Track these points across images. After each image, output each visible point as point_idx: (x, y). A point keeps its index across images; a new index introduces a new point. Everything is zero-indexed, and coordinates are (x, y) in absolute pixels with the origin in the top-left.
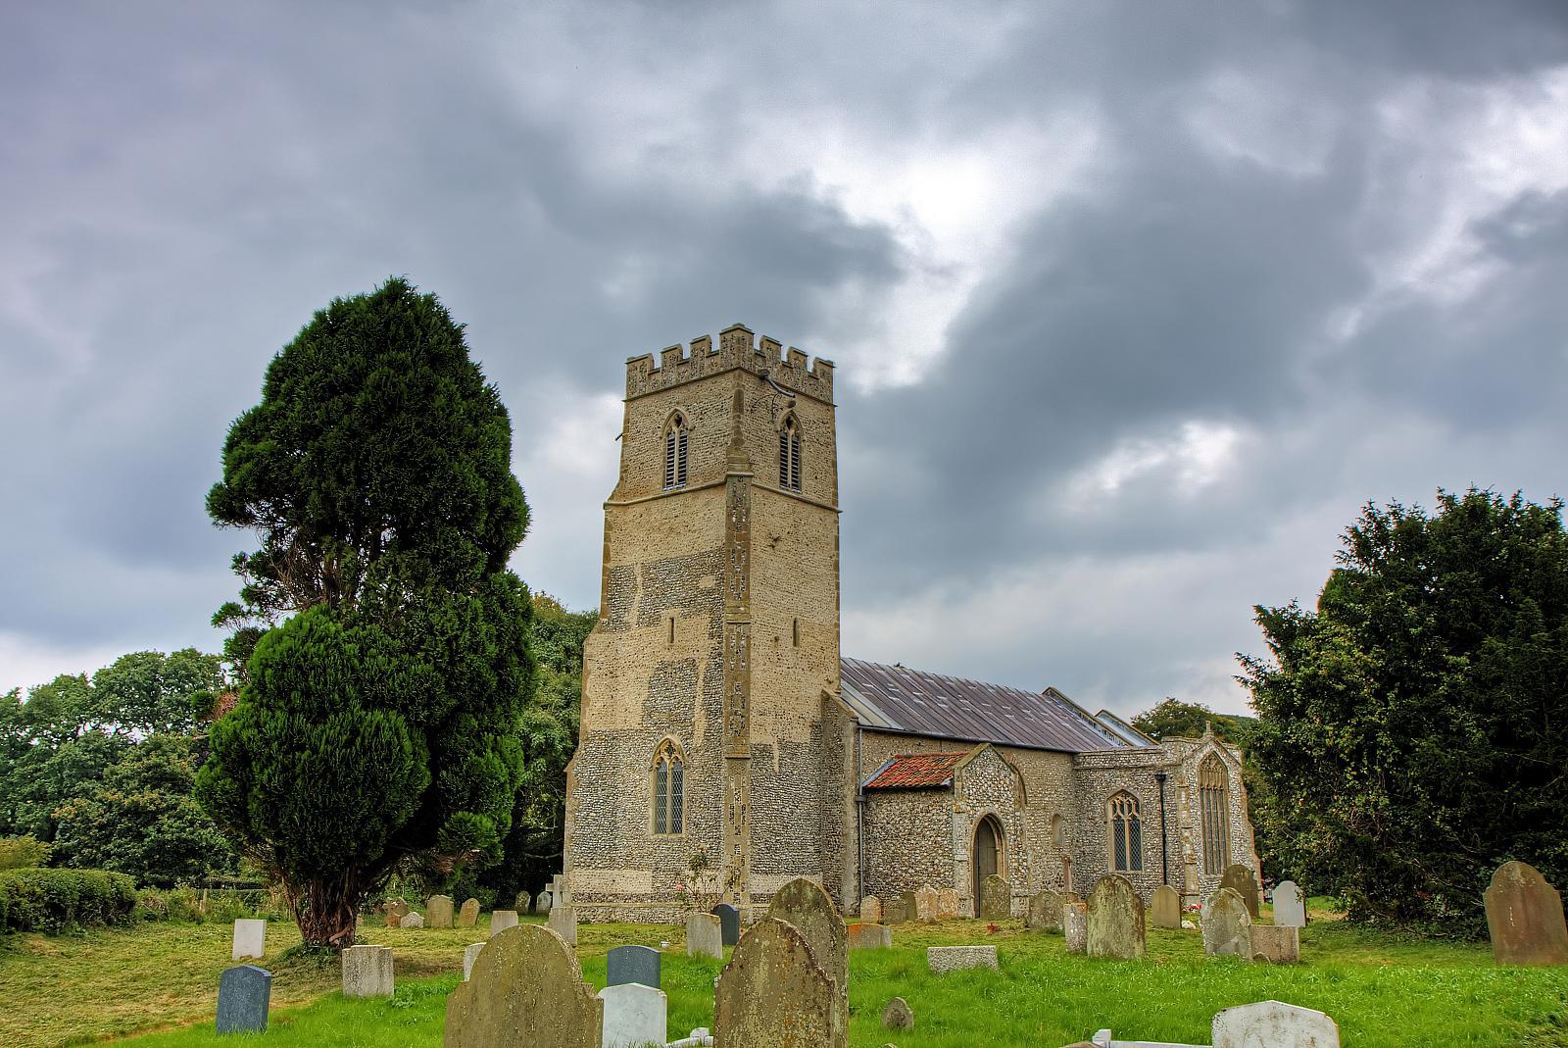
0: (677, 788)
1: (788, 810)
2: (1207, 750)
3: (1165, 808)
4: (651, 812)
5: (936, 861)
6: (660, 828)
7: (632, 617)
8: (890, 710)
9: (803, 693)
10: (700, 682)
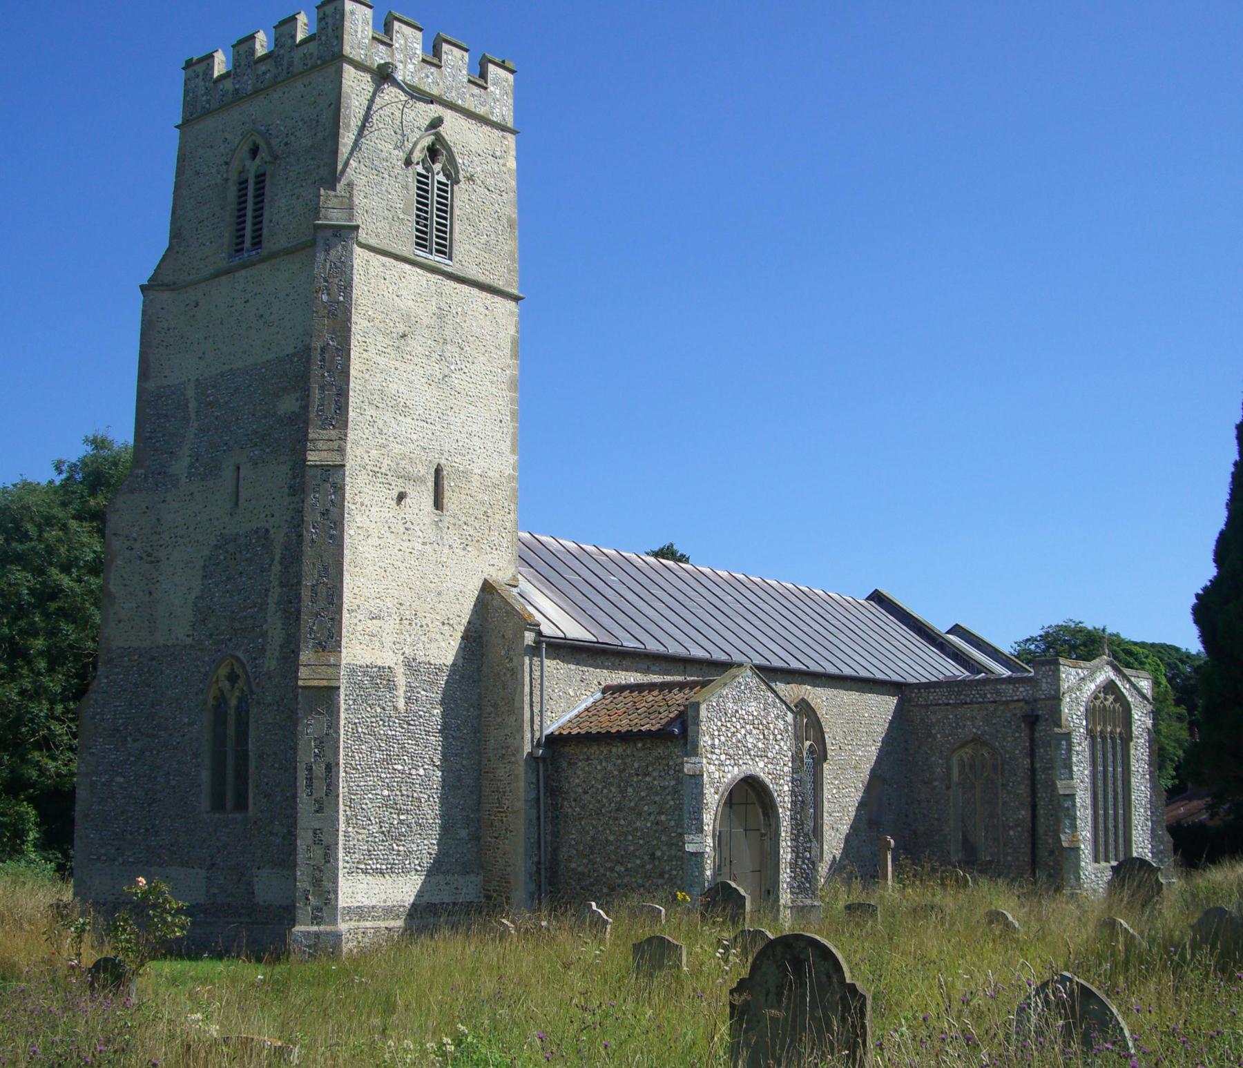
0: (242, 736)
1: (421, 772)
2: (1101, 678)
3: (1038, 765)
4: (205, 776)
5: (658, 853)
6: (218, 804)
7: (180, 467)
8: (578, 610)
9: (450, 585)
10: (277, 567)
